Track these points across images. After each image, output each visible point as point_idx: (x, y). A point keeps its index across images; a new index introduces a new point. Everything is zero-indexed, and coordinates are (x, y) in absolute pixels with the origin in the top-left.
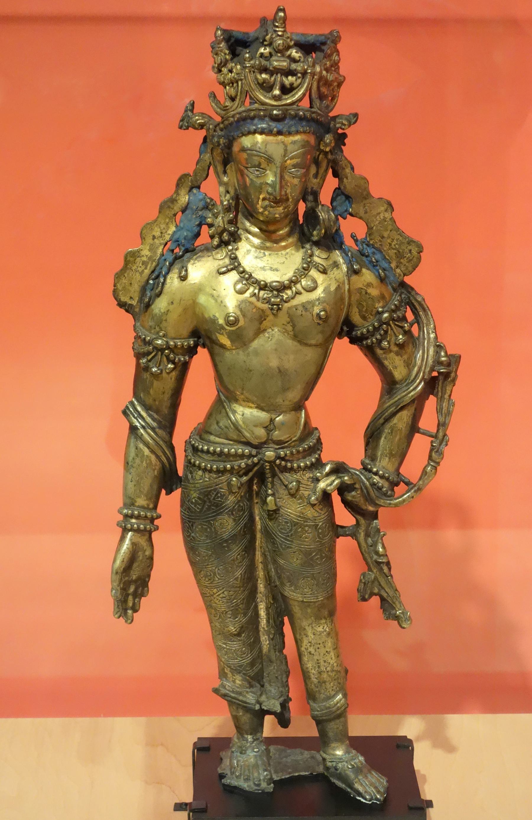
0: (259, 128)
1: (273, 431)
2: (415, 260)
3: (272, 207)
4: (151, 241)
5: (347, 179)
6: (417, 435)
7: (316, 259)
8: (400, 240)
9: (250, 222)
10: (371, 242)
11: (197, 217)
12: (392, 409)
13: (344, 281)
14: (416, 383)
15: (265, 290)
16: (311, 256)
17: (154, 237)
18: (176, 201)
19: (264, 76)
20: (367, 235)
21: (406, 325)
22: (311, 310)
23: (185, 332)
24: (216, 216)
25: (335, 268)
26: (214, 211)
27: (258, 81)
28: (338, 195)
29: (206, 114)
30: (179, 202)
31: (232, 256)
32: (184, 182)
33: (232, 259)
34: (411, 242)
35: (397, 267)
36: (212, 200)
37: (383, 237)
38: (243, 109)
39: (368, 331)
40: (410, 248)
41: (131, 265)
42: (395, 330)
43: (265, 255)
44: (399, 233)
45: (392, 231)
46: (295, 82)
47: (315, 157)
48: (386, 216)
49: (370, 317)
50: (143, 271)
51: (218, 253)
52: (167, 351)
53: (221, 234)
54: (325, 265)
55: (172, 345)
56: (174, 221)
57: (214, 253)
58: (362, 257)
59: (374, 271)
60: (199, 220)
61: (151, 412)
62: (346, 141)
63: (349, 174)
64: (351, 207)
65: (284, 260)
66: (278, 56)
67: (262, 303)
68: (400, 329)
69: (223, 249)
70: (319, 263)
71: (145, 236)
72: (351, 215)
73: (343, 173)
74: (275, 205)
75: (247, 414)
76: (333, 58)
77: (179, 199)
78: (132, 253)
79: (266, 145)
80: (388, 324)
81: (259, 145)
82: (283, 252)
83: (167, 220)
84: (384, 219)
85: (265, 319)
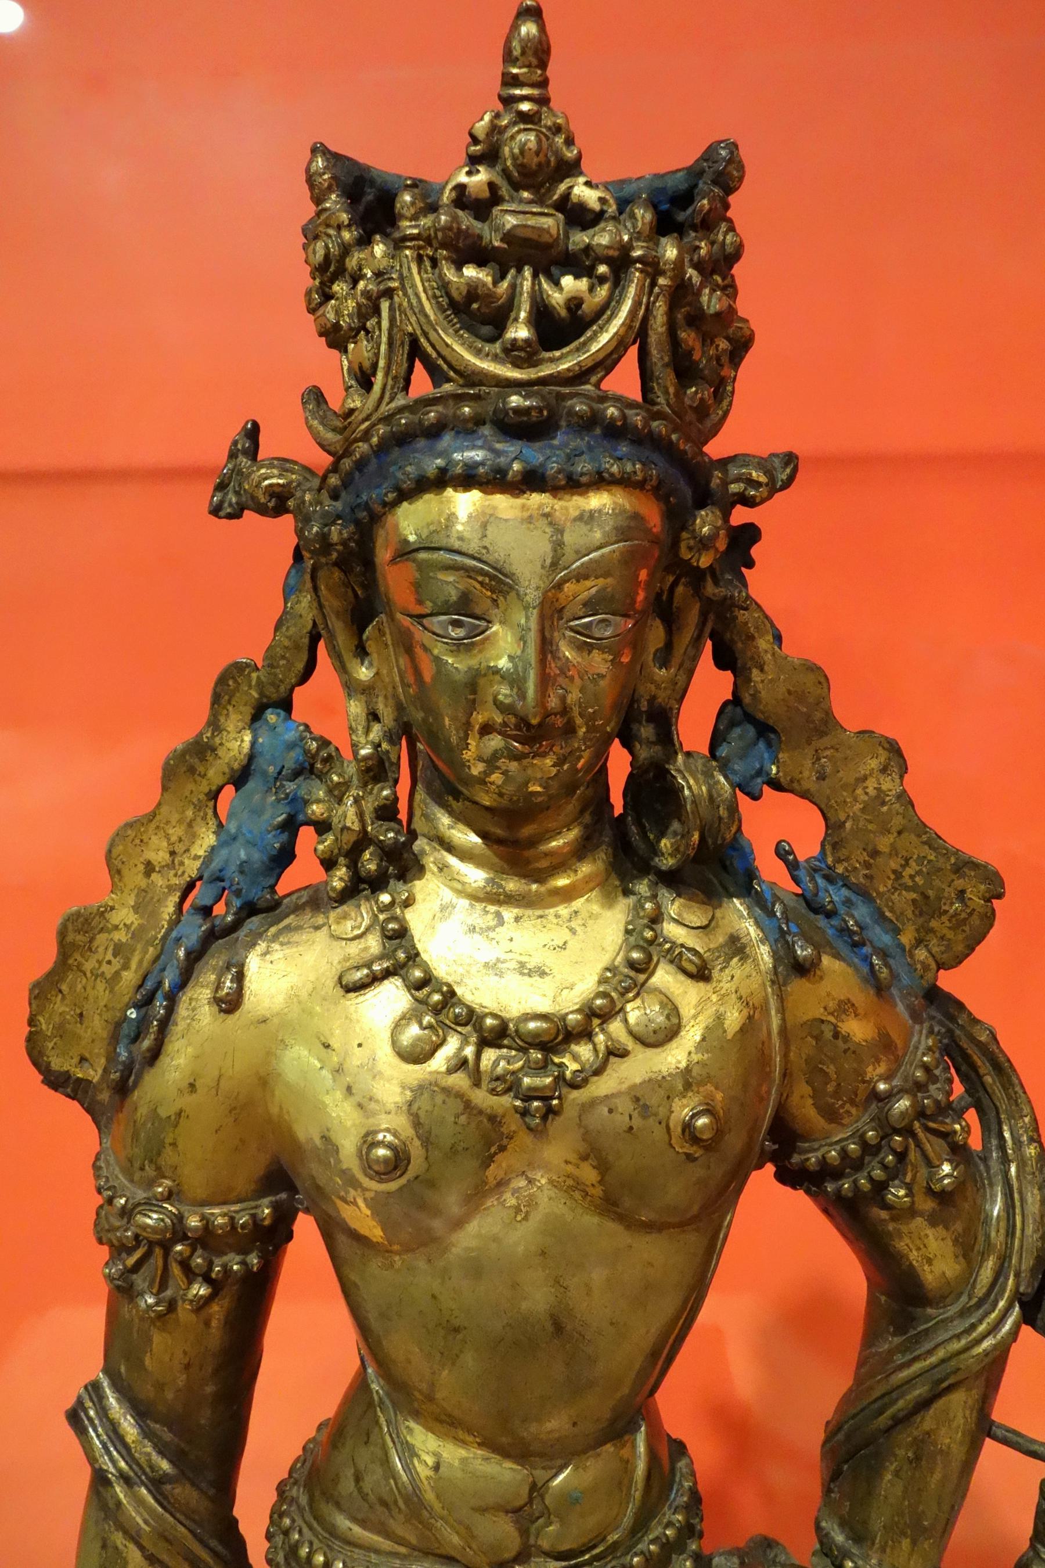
0: (458, 462)
1: (541, 1521)
2: (975, 920)
3: (517, 757)
4: (141, 881)
5: (762, 670)
6: (989, 1445)
7: (671, 930)
8: (930, 861)
9: (451, 813)
10: (840, 870)
11: (278, 801)
12: (919, 1391)
13: (766, 1000)
14: (997, 1312)
15: (500, 1047)
16: (656, 920)
17: (149, 868)
18: (214, 750)
19: (470, 272)
20: (828, 847)
21: (957, 1127)
22: (662, 1111)
23: (244, 1180)
24: (337, 793)
25: (735, 960)
26: (332, 781)
27: (448, 295)
28: (733, 724)
29: (295, 463)
30: (221, 752)
31: (390, 926)
32: (237, 689)
33: (390, 938)
34: (964, 865)
35: (919, 942)
36: (325, 743)
37: (875, 853)
38: (400, 401)
39: (844, 1153)
40: (960, 883)
41: (79, 958)
42: (928, 1147)
43: (501, 921)
44: (924, 838)
45: (905, 835)
46: (586, 296)
47: (659, 595)
48: (884, 787)
49: (848, 1112)
50: (117, 975)
51: (345, 917)
52: (179, 1248)
53: (353, 854)
54: (701, 951)
55: (196, 1228)
56: (210, 812)
57: (333, 915)
58: (812, 916)
59: (856, 960)
60: (288, 809)
61: (152, 1425)
62: (755, 551)
63: (769, 656)
64: (775, 761)
65: (566, 935)
66: (521, 201)
67: (493, 1092)
68: (941, 1141)
69: (362, 902)
70: (682, 946)
71: (120, 866)
72: (776, 785)
73: (749, 654)
74: (526, 749)
75: (451, 1465)
76: (721, 237)
77: (221, 744)
78: (81, 919)
79: (484, 526)
80: (908, 1132)
81: (460, 527)
82: (563, 910)
83: (190, 813)
84: (877, 797)
85: (502, 1149)
